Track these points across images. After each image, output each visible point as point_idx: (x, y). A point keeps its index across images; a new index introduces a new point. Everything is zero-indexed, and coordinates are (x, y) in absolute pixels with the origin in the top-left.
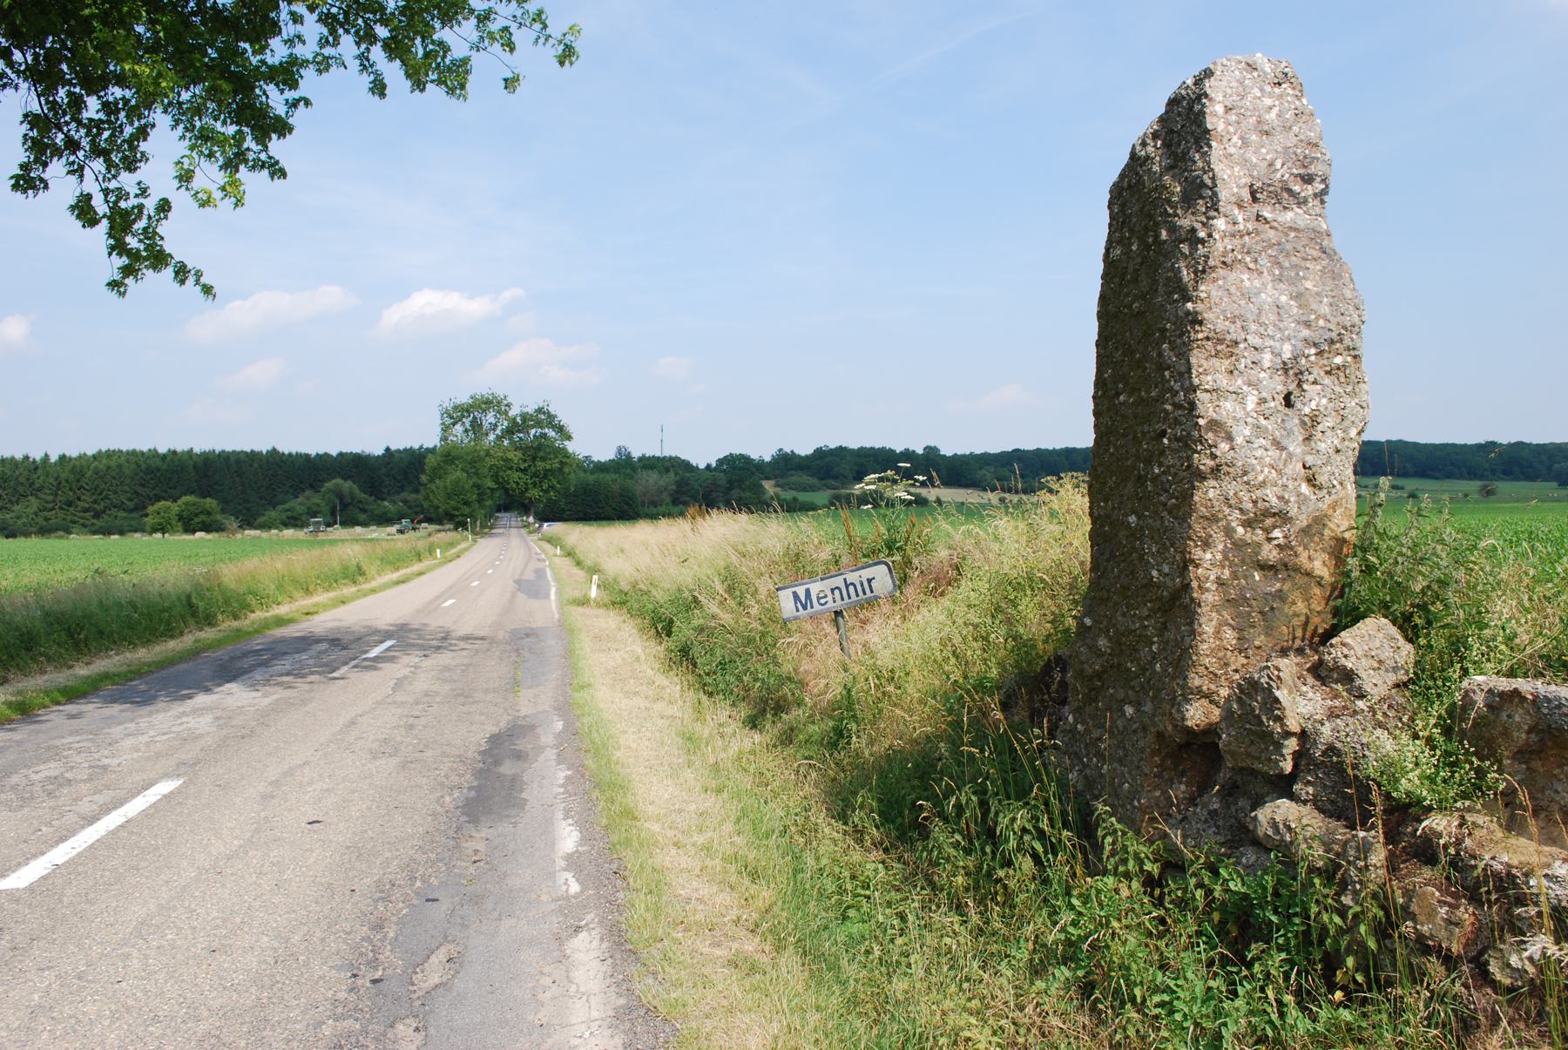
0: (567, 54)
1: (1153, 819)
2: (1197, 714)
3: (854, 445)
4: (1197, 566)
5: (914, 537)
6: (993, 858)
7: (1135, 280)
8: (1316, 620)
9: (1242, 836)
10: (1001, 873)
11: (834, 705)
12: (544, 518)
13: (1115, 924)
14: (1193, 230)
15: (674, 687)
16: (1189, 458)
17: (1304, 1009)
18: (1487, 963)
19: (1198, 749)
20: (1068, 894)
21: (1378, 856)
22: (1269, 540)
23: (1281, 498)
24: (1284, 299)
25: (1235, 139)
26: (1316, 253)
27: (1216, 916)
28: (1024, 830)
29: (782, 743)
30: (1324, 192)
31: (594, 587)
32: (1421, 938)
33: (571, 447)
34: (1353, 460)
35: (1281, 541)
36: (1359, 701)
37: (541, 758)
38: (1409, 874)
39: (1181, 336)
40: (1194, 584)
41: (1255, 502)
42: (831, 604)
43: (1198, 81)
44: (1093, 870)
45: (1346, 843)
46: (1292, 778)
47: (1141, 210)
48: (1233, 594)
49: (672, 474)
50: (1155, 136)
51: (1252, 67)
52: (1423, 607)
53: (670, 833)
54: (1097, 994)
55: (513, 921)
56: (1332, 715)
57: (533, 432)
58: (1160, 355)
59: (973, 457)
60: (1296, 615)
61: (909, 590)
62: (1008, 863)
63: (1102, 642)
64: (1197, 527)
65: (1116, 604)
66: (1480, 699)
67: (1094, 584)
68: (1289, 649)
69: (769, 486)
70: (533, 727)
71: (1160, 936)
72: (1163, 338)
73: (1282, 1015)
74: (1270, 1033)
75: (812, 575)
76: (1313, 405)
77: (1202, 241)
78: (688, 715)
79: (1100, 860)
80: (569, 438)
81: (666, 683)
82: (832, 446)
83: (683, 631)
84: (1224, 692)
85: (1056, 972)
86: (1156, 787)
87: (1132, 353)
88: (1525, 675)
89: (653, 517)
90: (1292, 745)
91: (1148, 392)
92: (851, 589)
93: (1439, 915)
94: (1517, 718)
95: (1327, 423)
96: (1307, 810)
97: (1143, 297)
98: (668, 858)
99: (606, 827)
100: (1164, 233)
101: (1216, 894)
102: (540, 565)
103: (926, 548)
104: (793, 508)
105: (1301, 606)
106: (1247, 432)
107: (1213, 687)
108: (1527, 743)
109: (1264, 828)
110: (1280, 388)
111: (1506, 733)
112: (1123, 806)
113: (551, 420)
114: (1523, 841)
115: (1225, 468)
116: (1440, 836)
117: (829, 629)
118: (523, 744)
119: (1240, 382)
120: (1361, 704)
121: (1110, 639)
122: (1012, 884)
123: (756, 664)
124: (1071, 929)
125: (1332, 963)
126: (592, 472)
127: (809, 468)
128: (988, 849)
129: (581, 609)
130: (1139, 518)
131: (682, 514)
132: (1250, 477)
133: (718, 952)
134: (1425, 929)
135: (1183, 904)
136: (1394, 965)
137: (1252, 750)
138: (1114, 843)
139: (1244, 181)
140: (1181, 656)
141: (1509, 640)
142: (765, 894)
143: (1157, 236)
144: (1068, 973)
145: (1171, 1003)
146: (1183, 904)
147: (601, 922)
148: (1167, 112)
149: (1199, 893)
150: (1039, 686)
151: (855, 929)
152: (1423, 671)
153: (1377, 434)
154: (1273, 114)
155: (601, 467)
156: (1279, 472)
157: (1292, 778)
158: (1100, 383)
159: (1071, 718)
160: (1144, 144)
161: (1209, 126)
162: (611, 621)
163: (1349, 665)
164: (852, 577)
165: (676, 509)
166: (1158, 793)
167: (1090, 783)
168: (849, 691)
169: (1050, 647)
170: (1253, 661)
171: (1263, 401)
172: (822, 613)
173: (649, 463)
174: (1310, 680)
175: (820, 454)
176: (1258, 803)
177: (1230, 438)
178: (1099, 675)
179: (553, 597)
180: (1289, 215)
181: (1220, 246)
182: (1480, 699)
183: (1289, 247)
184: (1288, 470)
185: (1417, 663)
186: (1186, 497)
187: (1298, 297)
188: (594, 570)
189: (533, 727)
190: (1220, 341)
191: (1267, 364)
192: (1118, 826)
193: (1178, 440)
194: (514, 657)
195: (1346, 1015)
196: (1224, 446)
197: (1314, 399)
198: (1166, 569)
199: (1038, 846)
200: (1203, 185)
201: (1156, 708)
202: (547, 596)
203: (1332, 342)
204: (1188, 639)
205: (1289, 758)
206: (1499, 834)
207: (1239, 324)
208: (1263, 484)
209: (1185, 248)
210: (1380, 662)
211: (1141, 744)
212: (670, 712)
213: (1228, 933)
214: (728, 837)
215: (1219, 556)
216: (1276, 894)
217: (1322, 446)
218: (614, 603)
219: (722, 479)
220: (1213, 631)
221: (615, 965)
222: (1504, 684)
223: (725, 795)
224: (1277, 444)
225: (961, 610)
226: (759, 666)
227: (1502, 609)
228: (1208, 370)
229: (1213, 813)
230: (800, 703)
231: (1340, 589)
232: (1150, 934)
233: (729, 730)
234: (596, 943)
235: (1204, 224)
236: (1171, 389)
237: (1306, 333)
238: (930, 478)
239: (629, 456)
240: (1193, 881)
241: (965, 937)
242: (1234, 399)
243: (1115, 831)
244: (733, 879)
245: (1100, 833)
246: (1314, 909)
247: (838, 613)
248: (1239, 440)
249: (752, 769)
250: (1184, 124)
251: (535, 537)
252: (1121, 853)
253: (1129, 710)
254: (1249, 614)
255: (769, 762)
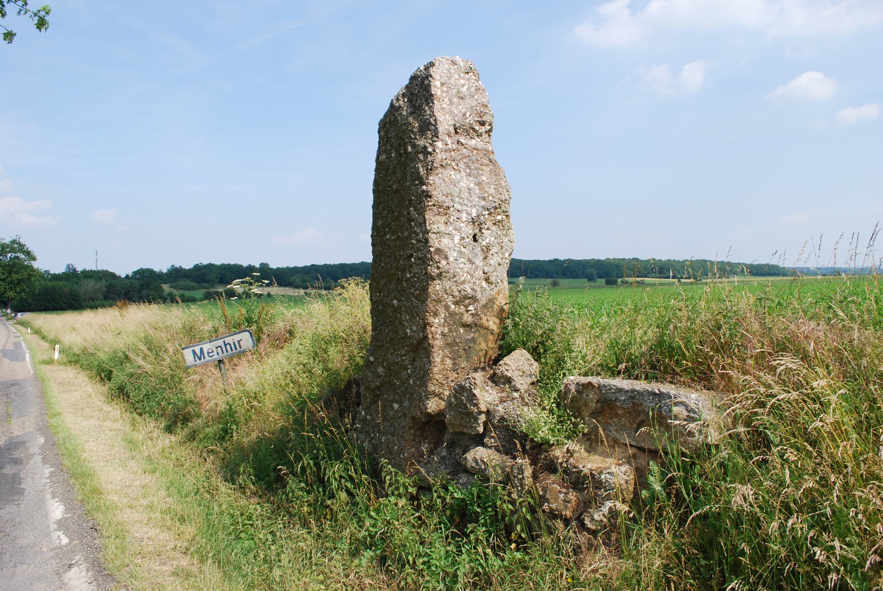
0: (41, 24)
1: (412, 464)
2: (433, 405)
3: (218, 262)
4: (431, 326)
5: (263, 316)
6: (324, 495)
7: (394, 173)
8: (491, 352)
9: (459, 468)
10: (329, 502)
11: (222, 415)
12: (17, 310)
13: (396, 523)
14: (425, 147)
15: (116, 411)
16: (426, 269)
17: (497, 555)
18: (584, 519)
19: (434, 425)
20: (367, 509)
21: (528, 472)
22: (467, 311)
23: (473, 289)
24: (472, 185)
25: (446, 100)
26: (487, 162)
27: (448, 512)
28: (341, 477)
29: (189, 440)
30: (490, 131)
31: (57, 353)
32: (552, 510)
33: (35, 265)
34: (507, 269)
35: (473, 312)
36: (514, 393)
37: (32, 462)
38: (544, 479)
39: (421, 202)
40: (430, 336)
41: (460, 292)
42: (216, 356)
43: (427, 68)
44: (379, 495)
45: (513, 466)
46: (484, 435)
47: (397, 135)
48: (450, 340)
49: (104, 281)
50: (404, 95)
51: (454, 63)
52: (542, 343)
53: (125, 500)
54: (389, 562)
55: (24, 567)
56: (502, 401)
57: (9, 255)
58: (409, 213)
59: (288, 269)
60: (481, 350)
61: (261, 347)
62: (332, 496)
63: (380, 370)
64: (431, 306)
65: (387, 348)
66: (573, 388)
67: (374, 338)
68: (478, 368)
69: (166, 288)
70: (24, 443)
71: (420, 527)
72: (410, 205)
73: (487, 559)
74: (481, 570)
75: (201, 340)
76: (487, 241)
77: (430, 154)
78: (128, 428)
79: (384, 489)
80: (34, 259)
81: (110, 409)
82: (205, 263)
83: (120, 376)
84: (447, 393)
85: (365, 554)
86: (413, 446)
87: (393, 212)
88: (592, 375)
89: (93, 307)
90: (483, 418)
91: (402, 233)
92: (228, 347)
93: (562, 498)
94: (591, 396)
95: (494, 250)
96: (491, 452)
97: (399, 182)
98: (126, 516)
99: (82, 501)
100: (410, 148)
101: (448, 501)
102: (17, 340)
103: (271, 321)
104: (187, 300)
105: (483, 346)
106: (455, 255)
107: (441, 390)
108: (596, 408)
109: (470, 463)
110: (471, 232)
111: (586, 404)
112: (394, 458)
113: (21, 248)
114: (596, 457)
115: (444, 274)
116: (558, 458)
117: (216, 372)
118: (17, 454)
119: (451, 228)
120: (516, 395)
121: (384, 368)
122: (335, 508)
123: (168, 394)
124: (371, 529)
125: (509, 529)
126: (50, 280)
127: (191, 276)
128: (321, 490)
129: (48, 367)
130: (399, 301)
131: (111, 306)
132: (457, 278)
133: (165, 568)
134: (554, 506)
135: (431, 508)
136: (540, 528)
137: (463, 422)
138: (391, 479)
139: (451, 122)
140: (424, 376)
141: (583, 357)
142: (190, 530)
143: (406, 149)
144: (371, 553)
145: (429, 561)
146: (431, 508)
147: (85, 560)
148: (410, 83)
149: (439, 501)
150: (344, 396)
151: (247, 544)
152: (544, 375)
153: (516, 256)
154: (465, 89)
155: (56, 277)
156: (472, 276)
157: (484, 435)
158: (375, 228)
159: (363, 413)
160: (398, 100)
161: (433, 93)
162: (70, 373)
163: (509, 375)
164: (228, 340)
165: (107, 303)
166: (413, 450)
167: (375, 448)
168: (230, 406)
169: (347, 375)
170: (461, 375)
171: (462, 238)
172: (209, 361)
173: (88, 275)
174: (490, 384)
175: (197, 268)
176: (466, 450)
177: (446, 258)
178: (378, 388)
179: (28, 359)
180: (473, 142)
181: (440, 156)
182: (573, 388)
183: (474, 158)
184: (476, 275)
185: (540, 372)
186: (425, 290)
187: (479, 184)
188: (54, 342)
189: (24, 443)
190: (441, 207)
191: (464, 219)
192: (393, 470)
193: (420, 259)
194: (5, 399)
195: (518, 555)
196: (444, 262)
197: (488, 238)
198: (415, 328)
199: (349, 485)
200: (430, 123)
201: (411, 403)
202: (24, 360)
203: (496, 208)
204: (427, 366)
205: (482, 425)
206: (586, 454)
207: (450, 198)
208: (463, 282)
209: (421, 156)
210: (523, 372)
211: (403, 424)
212: (115, 426)
213: (455, 520)
214: (161, 498)
215: (442, 321)
216: (479, 497)
217: (492, 262)
218: (70, 362)
219: (136, 284)
220: (440, 360)
221: (98, 585)
222: (584, 380)
223: (158, 474)
224: (470, 261)
225: (295, 356)
226: (171, 395)
227: (579, 342)
228: (434, 222)
229: (443, 458)
230: (199, 416)
231: (503, 336)
232: (414, 526)
233: (155, 435)
234: (84, 573)
235: (431, 144)
236: (415, 232)
237: (483, 203)
238: (272, 281)
239: (75, 270)
240: (435, 495)
241: (310, 540)
242: (447, 236)
243: (391, 472)
244: (169, 523)
245: (383, 474)
246: (499, 503)
247: (220, 361)
248: (451, 259)
249: (173, 456)
250: (419, 90)
251: (12, 322)
252: (395, 483)
253: (396, 406)
254: (458, 351)
255: (183, 452)
